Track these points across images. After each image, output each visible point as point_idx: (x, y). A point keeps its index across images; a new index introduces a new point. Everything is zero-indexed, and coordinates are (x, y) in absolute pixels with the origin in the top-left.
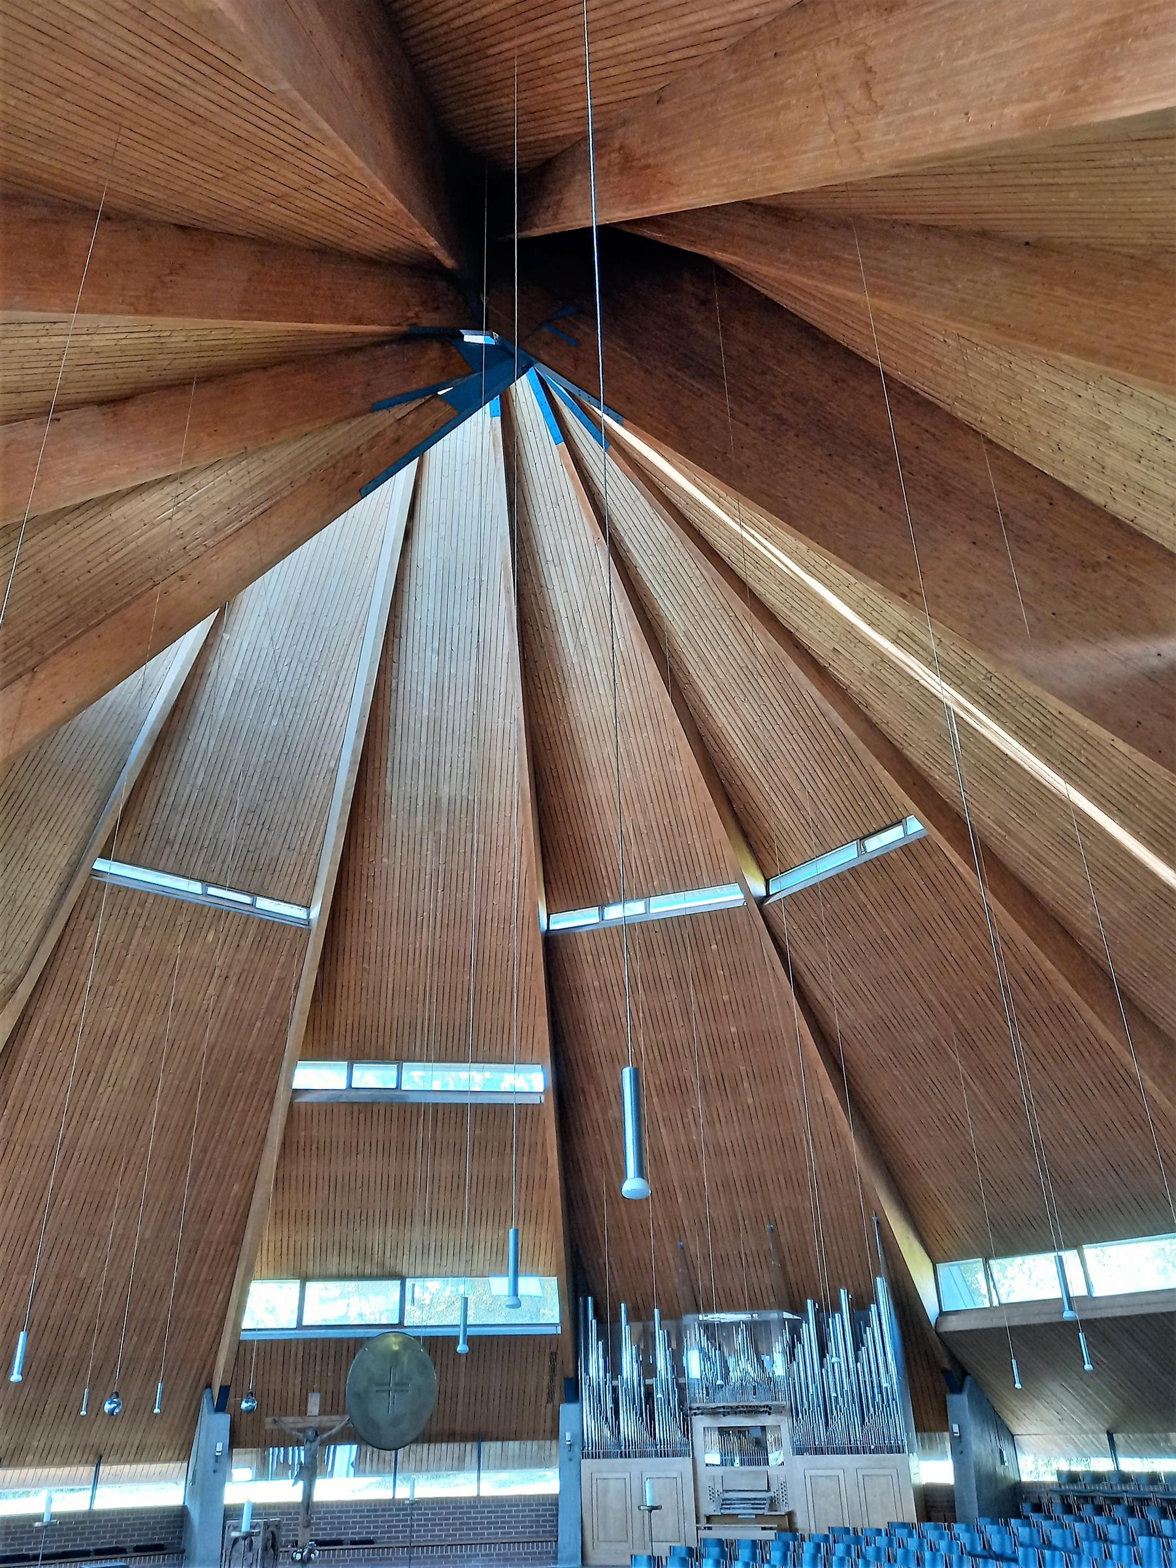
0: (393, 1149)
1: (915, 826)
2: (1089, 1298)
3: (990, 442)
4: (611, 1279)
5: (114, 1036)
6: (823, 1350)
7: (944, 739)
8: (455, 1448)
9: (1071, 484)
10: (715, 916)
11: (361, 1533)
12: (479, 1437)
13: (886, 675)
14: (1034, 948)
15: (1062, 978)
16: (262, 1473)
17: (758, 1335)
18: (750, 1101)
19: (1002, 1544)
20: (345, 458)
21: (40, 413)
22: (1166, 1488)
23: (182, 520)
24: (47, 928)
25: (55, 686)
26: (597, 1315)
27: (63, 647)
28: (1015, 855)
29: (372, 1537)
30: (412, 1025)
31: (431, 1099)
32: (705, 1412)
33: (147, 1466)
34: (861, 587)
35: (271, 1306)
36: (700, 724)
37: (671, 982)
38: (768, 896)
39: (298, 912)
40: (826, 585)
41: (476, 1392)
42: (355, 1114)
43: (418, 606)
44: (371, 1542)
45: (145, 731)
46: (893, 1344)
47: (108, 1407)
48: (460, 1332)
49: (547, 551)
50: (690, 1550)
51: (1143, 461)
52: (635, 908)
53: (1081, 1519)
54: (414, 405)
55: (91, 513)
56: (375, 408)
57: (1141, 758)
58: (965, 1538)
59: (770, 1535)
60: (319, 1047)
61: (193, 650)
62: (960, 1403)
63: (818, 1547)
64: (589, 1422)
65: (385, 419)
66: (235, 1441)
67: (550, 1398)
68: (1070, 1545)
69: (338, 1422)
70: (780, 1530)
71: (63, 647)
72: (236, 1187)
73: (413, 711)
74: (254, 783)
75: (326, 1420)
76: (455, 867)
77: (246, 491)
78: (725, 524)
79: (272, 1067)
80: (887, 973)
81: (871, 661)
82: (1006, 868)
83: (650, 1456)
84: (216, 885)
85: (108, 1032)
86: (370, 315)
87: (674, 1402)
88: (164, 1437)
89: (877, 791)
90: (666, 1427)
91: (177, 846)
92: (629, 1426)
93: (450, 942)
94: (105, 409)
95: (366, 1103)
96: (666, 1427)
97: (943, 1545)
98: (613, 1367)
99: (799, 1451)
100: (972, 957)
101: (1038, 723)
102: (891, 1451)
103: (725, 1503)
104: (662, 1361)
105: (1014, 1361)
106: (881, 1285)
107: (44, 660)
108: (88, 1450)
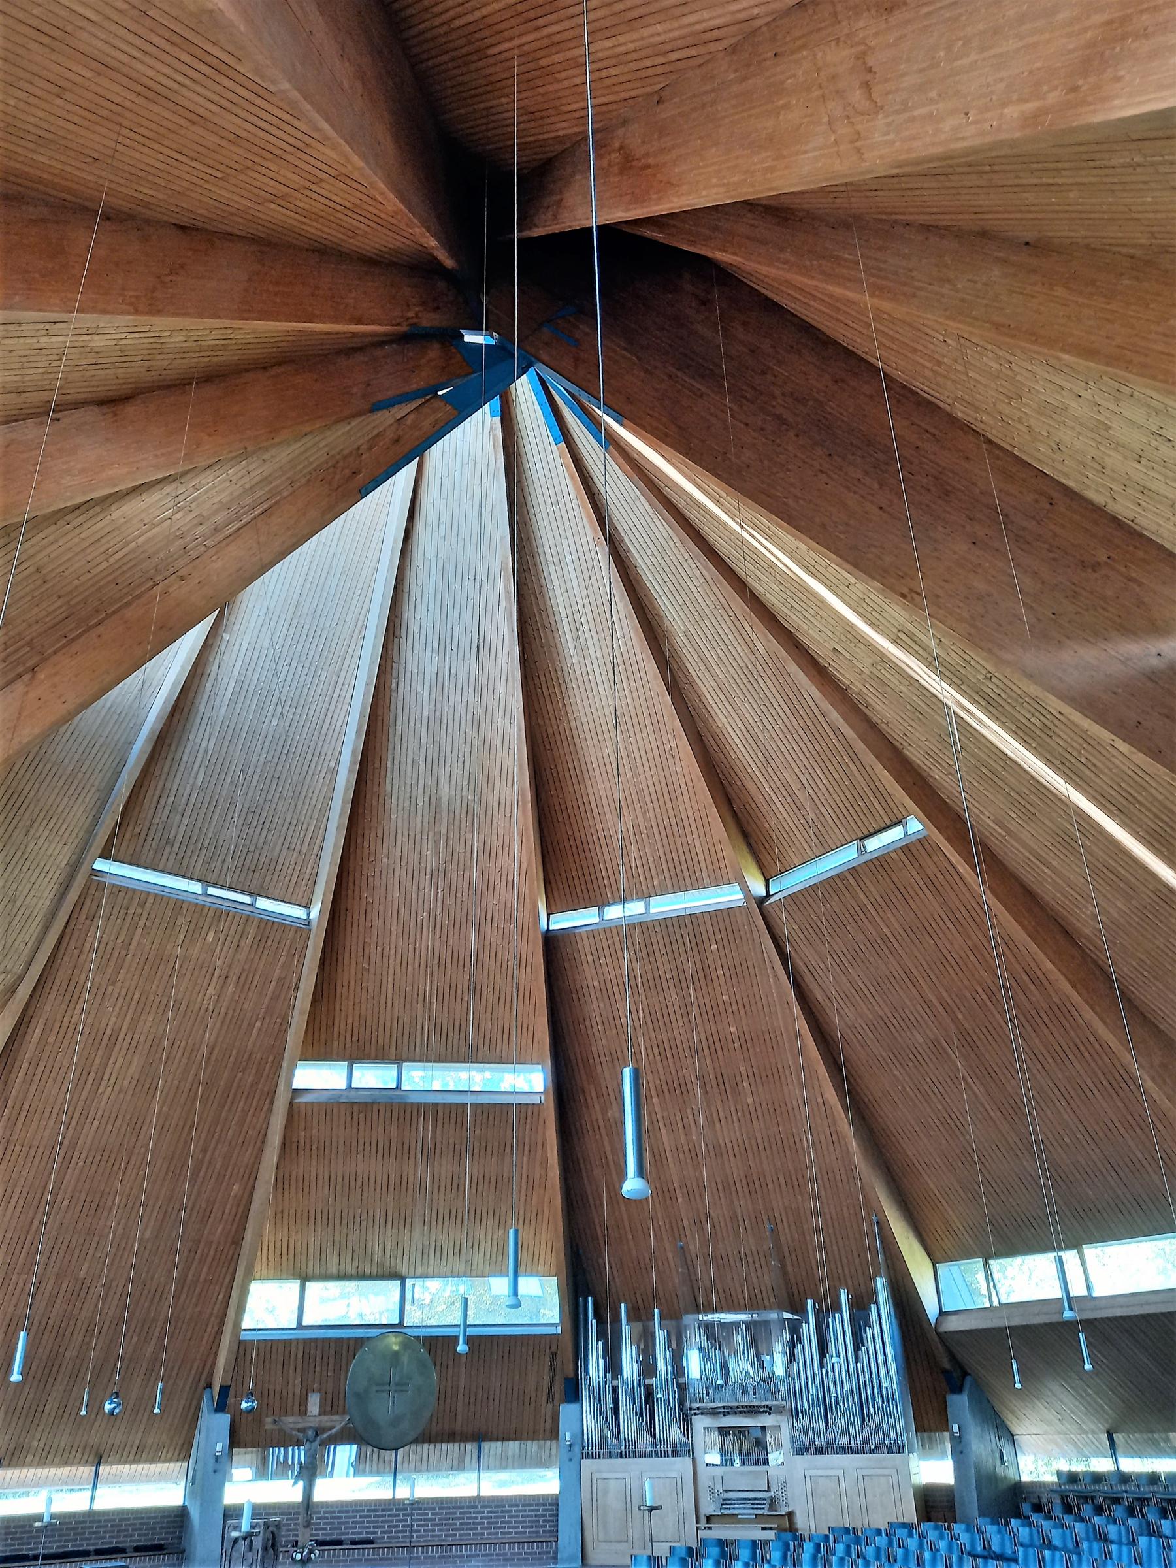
0: (393, 1149)
1: (915, 826)
2: (1089, 1298)
3: (990, 442)
4: (611, 1279)
5: (114, 1036)
6: (823, 1350)
7: (944, 739)
8: (455, 1448)
9: (1071, 484)
10: (715, 916)
11: (361, 1533)
12: (479, 1437)
13: (886, 675)
14: (1034, 948)
15: (1062, 978)
16: (262, 1473)
17: (758, 1335)
18: (750, 1101)
19: (1002, 1544)
20: (345, 458)
21: (40, 413)
22: (1166, 1488)
23: (182, 520)
24: (47, 928)
25: (55, 686)
26: (597, 1315)
27: (63, 647)
28: (1015, 855)
29: (372, 1537)
30: (412, 1025)
31: (431, 1099)
32: (705, 1412)
33: (147, 1466)
34: (861, 587)
35: (271, 1306)
36: (700, 724)
37: (671, 982)
38: (768, 896)
39: (298, 912)
40: (826, 585)
41: (476, 1392)
42: (355, 1114)
43: (418, 606)
44: (371, 1542)
45: (145, 731)
46: (893, 1344)
47: (108, 1407)
48: (460, 1332)
49: (547, 551)
50: (690, 1550)
51: (1143, 461)
52: (635, 908)
53: (1081, 1519)
54: (414, 405)
55: (91, 513)
56: (375, 408)
57: (1141, 758)
58: (965, 1538)
59: (770, 1535)
60: (319, 1047)
61: (193, 650)
62: (960, 1403)
63: (818, 1547)
64: (589, 1422)
65: (385, 419)
66: (235, 1441)
67: (550, 1398)
68: (1070, 1545)
69: (338, 1422)
70: (780, 1530)
71: (63, 647)
72: (236, 1187)
73: (413, 711)
74: (254, 783)
75: (326, 1420)
76: (455, 867)
77: (246, 491)
78: (725, 524)
79: (272, 1067)
80: (887, 973)
81: (871, 661)
82: (1006, 868)
83: (650, 1456)
84: (216, 885)
85: (108, 1032)
86: (370, 315)
87: (674, 1402)
88: (164, 1437)
89: (877, 791)
90: (666, 1427)
91: (177, 846)
92: (629, 1426)
93: (450, 942)
94: (105, 409)
95: (366, 1103)
96: (666, 1427)
97: (943, 1545)
98: (613, 1367)
99: (799, 1451)
100: (972, 957)
101: (1038, 723)
102: (891, 1451)
103: (725, 1503)
104: (662, 1361)
105: (1014, 1361)
106: (881, 1285)
107: (44, 660)
108: (88, 1450)
